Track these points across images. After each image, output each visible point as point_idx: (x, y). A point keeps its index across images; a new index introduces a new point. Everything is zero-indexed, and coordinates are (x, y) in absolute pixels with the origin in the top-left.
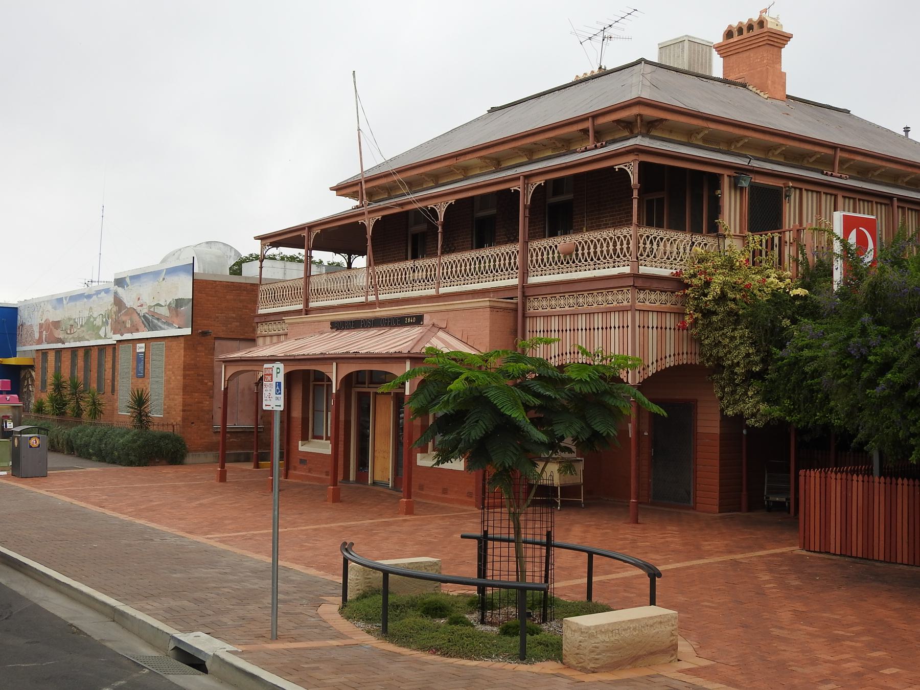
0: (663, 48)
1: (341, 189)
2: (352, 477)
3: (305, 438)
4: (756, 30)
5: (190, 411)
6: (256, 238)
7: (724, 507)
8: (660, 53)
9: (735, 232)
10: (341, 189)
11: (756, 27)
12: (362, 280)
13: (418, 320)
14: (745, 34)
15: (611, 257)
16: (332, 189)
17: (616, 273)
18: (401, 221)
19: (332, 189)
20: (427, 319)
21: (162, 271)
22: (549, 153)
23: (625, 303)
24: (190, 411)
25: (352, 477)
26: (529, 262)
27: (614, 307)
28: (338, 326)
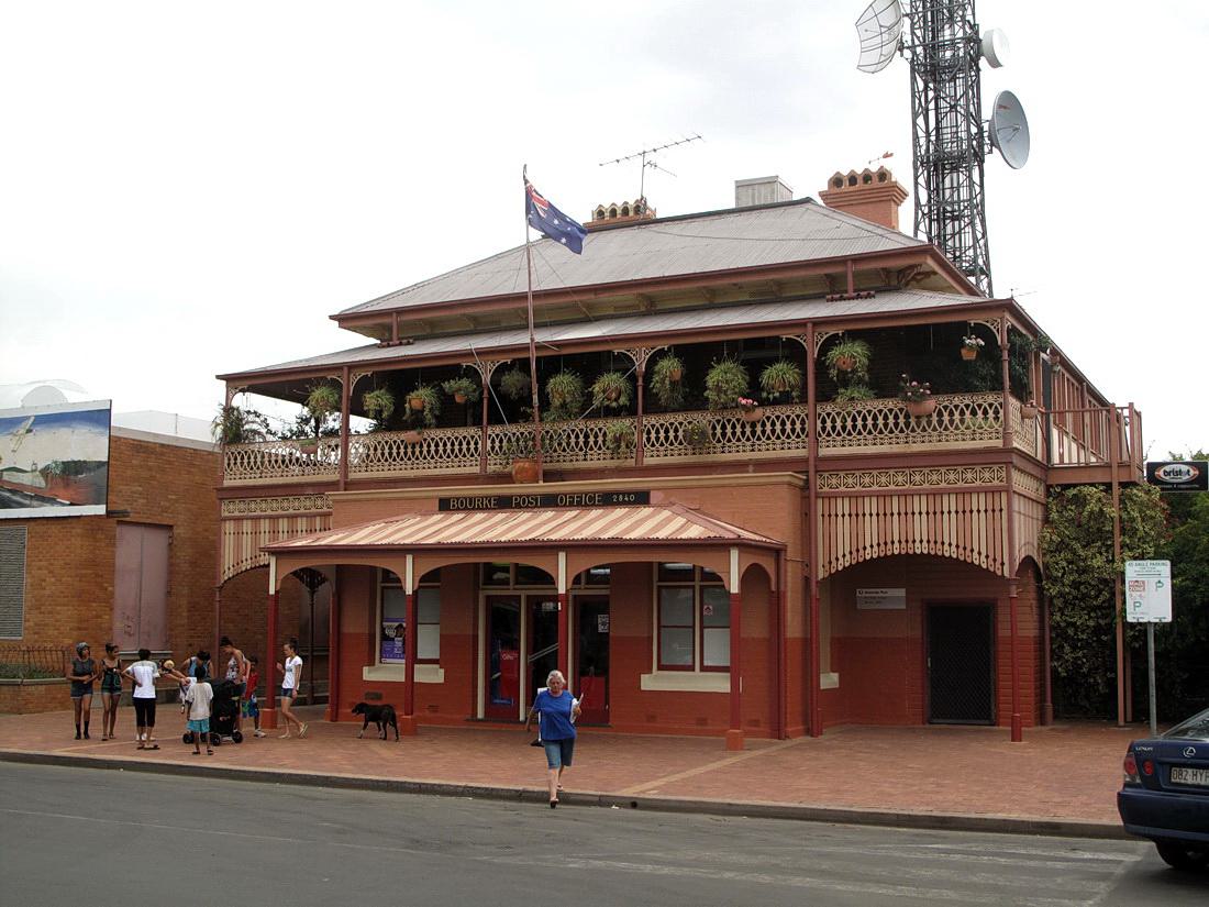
0: (741, 186)
1: (346, 320)
2: (480, 715)
3: (371, 663)
4: (875, 183)
5: (86, 629)
6: (218, 377)
7: (1056, 717)
8: (737, 194)
9: (1069, 407)
10: (346, 320)
11: (860, 181)
12: (356, 450)
13: (641, 499)
14: (860, 185)
15: (433, 458)
16: (332, 317)
17: (281, 482)
18: (431, 377)
19: (332, 317)
20: (655, 497)
21: (28, 418)
23: (996, 482)
24: (86, 629)
25: (480, 715)
26: (226, 465)
27: (888, 491)
28: (445, 506)
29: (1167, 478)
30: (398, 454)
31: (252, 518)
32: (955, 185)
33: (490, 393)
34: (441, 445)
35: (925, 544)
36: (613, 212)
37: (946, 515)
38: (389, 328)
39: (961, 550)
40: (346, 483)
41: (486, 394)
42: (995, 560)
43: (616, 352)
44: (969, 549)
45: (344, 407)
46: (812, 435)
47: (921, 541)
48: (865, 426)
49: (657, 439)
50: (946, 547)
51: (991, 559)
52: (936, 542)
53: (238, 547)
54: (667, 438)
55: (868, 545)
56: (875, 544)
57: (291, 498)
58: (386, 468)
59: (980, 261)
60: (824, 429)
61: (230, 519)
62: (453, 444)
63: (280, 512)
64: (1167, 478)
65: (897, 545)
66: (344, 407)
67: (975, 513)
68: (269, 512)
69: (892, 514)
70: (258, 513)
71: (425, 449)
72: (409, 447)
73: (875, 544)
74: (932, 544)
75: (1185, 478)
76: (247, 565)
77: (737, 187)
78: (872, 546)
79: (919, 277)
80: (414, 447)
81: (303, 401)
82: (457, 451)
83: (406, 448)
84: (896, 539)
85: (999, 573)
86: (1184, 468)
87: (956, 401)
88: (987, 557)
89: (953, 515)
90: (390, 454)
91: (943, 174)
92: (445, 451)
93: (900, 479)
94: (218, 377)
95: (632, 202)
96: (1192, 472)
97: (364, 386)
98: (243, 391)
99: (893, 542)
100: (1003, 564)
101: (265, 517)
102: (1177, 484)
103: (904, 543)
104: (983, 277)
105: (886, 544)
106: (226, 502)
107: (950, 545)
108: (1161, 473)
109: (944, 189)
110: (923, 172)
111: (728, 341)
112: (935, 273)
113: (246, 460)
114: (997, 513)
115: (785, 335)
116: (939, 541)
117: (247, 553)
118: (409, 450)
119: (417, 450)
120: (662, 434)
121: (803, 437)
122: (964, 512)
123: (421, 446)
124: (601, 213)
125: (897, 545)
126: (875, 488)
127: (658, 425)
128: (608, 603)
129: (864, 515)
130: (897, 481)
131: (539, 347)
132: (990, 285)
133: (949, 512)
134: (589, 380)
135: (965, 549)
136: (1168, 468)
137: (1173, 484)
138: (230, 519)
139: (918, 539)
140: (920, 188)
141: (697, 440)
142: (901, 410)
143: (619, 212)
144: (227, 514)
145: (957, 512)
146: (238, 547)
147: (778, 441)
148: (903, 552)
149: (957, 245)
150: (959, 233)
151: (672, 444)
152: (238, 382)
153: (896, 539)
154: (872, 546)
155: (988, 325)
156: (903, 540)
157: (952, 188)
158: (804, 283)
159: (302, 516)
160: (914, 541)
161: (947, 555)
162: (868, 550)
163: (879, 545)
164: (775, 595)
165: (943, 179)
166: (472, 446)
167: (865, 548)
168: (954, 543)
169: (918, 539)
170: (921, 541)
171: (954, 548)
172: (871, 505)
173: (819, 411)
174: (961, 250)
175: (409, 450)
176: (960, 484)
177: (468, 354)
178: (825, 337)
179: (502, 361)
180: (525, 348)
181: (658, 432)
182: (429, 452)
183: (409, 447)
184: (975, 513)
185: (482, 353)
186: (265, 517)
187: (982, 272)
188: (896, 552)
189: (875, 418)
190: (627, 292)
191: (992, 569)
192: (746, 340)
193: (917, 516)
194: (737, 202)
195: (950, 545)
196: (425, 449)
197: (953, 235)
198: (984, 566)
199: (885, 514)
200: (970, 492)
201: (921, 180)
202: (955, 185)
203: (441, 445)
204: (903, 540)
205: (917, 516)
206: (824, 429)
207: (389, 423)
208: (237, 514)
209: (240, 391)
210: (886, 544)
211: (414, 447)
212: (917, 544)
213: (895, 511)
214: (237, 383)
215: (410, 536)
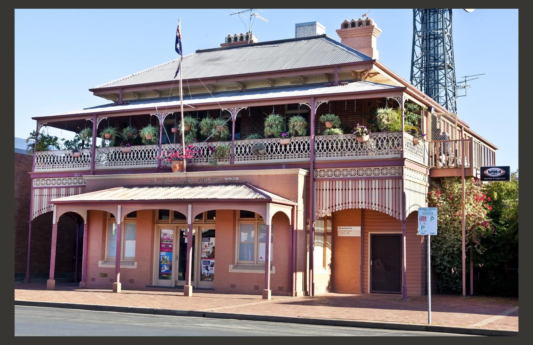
0: (298, 26)
1: (97, 92)
6: (33, 118)
10: (97, 92)
11: (357, 25)
22: (289, 84)
29: (490, 174)
30: (276, 150)
31: (48, 188)
32: (436, 20)
33: (163, 128)
34: (139, 153)
35: (364, 204)
36: (236, 38)
37: (374, 190)
38: (118, 96)
39: (380, 207)
40: (93, 172)
41: (161, 128)
42: (396, 212)
43: (223, 110)
44: (384, 206)
45: (94, 134)
46: (312, 151)
47: (362, 203)
48: (323, 148)
49: (241, 152)
50: (373, 205)
51: (394, 211)
52: (369, 203)
53: (41, 202)
54: (299, 149)
55: (337, 204)
56: (340, 204)
57: (41, 179)
58: (62, 166)
59: (448, 62)
60: (318, 148)
61: (37, 188)
62: (145, 153)
63: (62, 185)
64: (490, 174)
65: (350, 204)
66: (94, 134)
67: (337, 191)
68: (56, 185)
69: (349, 189)
70: (51, 185)
71: (132, 155)
72: (125, 154)
73: (340, 204)
74: (344, 204)
75: (499, 174)
76: (44, 211)
77: (296, 27)
78: (339, 205)
79: (371, 75)
80: (126, 154)
81: (77, 131)
82: (135, 157)
83: (123, 155)
84: (350, 201)
85: (397, 218)
86: (498, 170)
87: (380, 136)
88: (392, 210)
89: (377, 190)
90: (137, 157)
91: (429, 15)
92: (141, 156)
93: (353, 173)
94: (33, 118)
95: (244, 34)
96: (502, 172)
97: (104, 125)
98: (45, 125)
99: (349, 203)
100: (399, 214)
101: (54, 187)
102: (495, 177)
103: (344, 204)
104: (449, 70)
105: (345, 203)
106: (36, 180)
107: (375, 204)
108: (502, 172)
109: (430, 23)
110: (419, 13)
111: (209, 110)
112: (379, 73)
113: (45, 160)
114: (397, 189)
115: (302, 103)
116: (357, 202)
117: (45, 205)
118: (124, 156)
119: (128, 155)
120: (297, 147)
121: (308, 152)
122: (382, 189)
123: (130, 154)
124: (229, 39)
125: (350, 204)
126: (341, 176)
127: (295, 142)
128: (515, 248)
129: (385, 188)
130: (352, 172)
131: (185, 107)
132: (454, 74)
133: (375, 189)
134: (120, 129)
135: (379, 205)
136: (490, 170)
137: (492, 177)
138: (37, 188)
139: (360, 201)
140: (417, 23)
141: (256, 151)
142: (354, 140)
143: (233, 39)
144: (35, 186)
145: (379, 189)
146: (41, 202)
147: (243, 157)
148: (353, 208)
149: (436, 53)
150: (437, 46)
151: (139, 159)
152: (41, 121)
153: (350, 201)
154: (339, 205)
155: (396, 99)
156: (354, 202)
157: (434, 22)
158: (316, 77)
159: (45, 188)
160: (359, 203)
161: (374, 209)
162: (337, 206)
163: (342, 204)
164: (291, 227)
165: (430, 17)
166: (239, 150)
167: (336, 206)
168: (377, 204)
169: (360, 201)
170: (362, 203)
171: (377, 206)
172: (339, 185)
173: (316, 139)
174: (438, 56)
175: (124, 156)
176: (381, 175)
177: (153, 109)
178: (320, 104)
179: (169, 113)
180: (179, 107)
181: (149, 153)
182: (130, 157)
183: (125, 154)
184: (337, 190)
185: (160, 109)
186: (54, 187)
187: (449, 67)
188: (350, 208)
189: (299, 145)
190: (231, 80)
191: (394, 216)
192: (289, 105)
193: (325, 191)
194: (296, 35)
195: (375, 204)
196: (132, 155)
197: (434, 48)
198: (391, 215)
199: (345, 190)
200: (371, 179)
201: (418, 18)
202: (436, 20)
203: (139, 153)
204: (354, 202)
205: (325, 191)
206: (318, 148)
207: (118, 142)
208: (40, 186)
209: (44, 125)
210: (345, 203)
211: (126, 154)
212: (360, 204)
213: (350, 188)
214: (42, 122)
215: (165, 195)
